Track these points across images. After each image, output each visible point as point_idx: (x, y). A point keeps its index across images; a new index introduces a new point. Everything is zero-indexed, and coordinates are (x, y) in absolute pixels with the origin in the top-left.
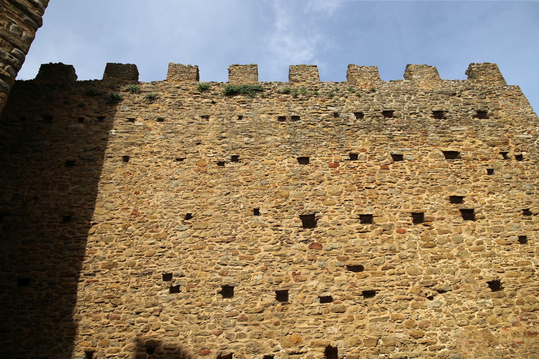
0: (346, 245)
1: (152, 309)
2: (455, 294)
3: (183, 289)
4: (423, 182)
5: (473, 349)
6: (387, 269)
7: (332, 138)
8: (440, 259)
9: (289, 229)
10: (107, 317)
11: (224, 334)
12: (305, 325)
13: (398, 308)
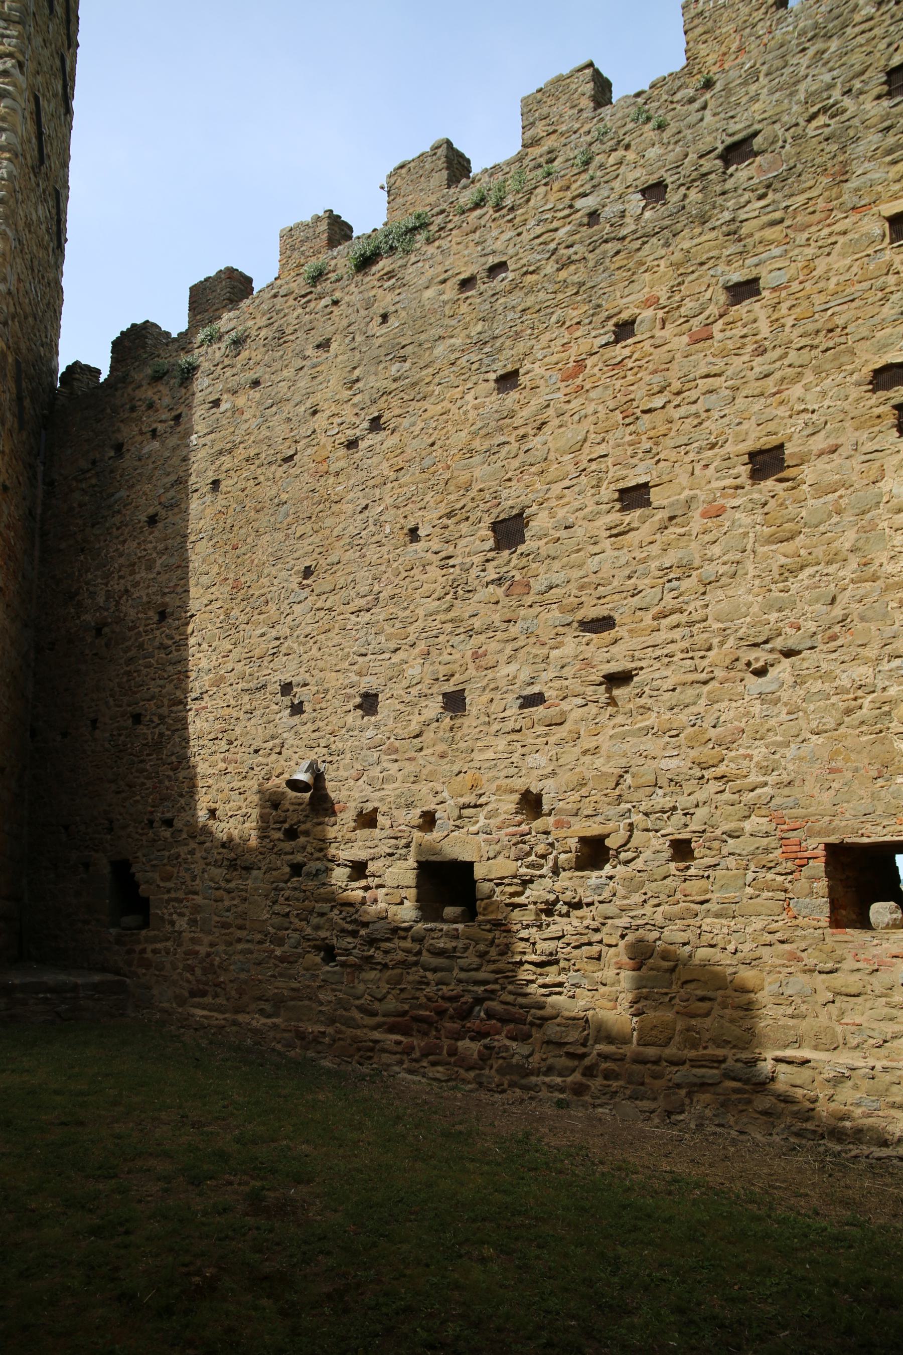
0: (581, 573)
1: (270, 744)
2: (823, 656)
3: (307, 707)
4: (799, 349)
5: (834, 785)
6: (665, 617)
7: (576, 293)
8: (802, 568)
9: (468, 560)
10: (224, 760)
11: (364, 778)
12: (490, 754)
13: (674, 703)
